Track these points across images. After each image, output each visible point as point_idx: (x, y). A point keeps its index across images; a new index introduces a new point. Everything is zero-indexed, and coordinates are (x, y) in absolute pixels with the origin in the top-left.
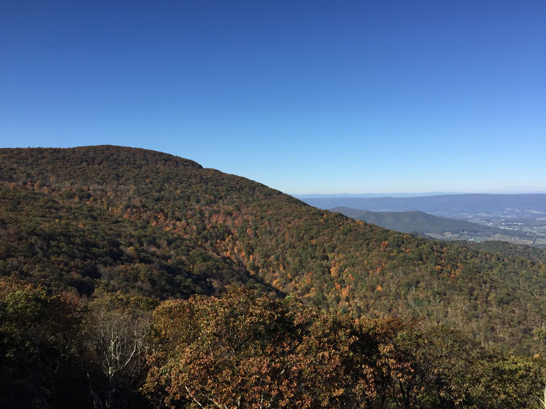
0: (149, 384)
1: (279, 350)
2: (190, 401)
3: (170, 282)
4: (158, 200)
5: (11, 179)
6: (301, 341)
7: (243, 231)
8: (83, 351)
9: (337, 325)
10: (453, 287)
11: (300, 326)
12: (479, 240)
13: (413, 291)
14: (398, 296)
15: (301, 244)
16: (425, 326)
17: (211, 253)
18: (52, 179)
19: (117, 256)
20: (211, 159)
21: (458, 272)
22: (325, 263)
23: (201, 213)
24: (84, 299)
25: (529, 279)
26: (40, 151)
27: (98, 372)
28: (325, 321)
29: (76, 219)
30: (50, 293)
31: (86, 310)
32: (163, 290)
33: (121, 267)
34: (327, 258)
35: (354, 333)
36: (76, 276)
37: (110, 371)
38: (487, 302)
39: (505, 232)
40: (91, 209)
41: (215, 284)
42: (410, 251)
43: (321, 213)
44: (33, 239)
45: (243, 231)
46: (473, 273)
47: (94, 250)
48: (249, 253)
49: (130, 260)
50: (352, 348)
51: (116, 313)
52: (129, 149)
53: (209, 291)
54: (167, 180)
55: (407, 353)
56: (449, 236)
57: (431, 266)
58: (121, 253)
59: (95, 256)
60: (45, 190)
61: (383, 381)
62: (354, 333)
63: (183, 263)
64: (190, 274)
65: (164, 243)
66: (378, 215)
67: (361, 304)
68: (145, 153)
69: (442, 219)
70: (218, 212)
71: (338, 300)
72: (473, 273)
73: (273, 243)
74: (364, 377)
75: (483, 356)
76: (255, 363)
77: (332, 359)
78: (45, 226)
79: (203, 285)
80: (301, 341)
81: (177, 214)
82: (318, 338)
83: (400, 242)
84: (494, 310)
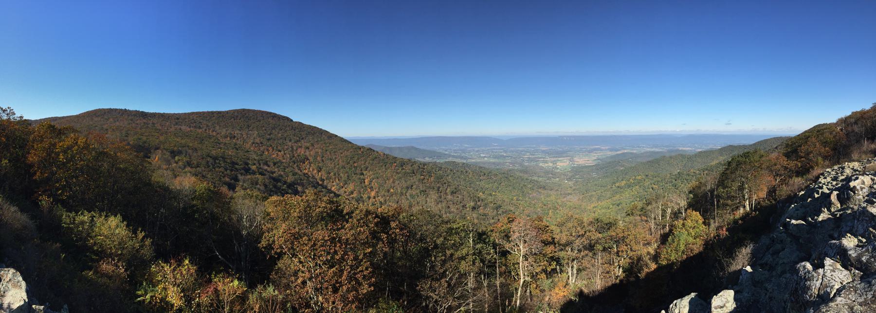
0: (264, 243)
1: (335, 227)
2: (285, 254)
3: (275, 186)
4: (269, 140)
5: (200, 128)
6: (347, 222)
7: (315, 158)
8: (230, 219)
9: (368, 213)
10: (430, 187)
11: (347, 214)
12: (442, 161)
13: (410, 191)
14: (402, 194)
15: (348, 166)
16: (415, 209)
17: (297, 171)
18: (218, 128)
19: (247, 171)
20: (297, 117)
21: (432, 179)
22: (362, 177)
23: (292, 147)
24: (231, 192)
25: (465, 180)
26: (212, 113)
27: (238, 233)
28: (361, 211)
29: (228, 149)
30: (215, 187)
31: (232, 198)
32: (271, 191)
33: (249, 177)
34: (362, 174)
35: (377, 216)
36: (227, 180)
37: (244, 232)
38: (446, 193)
39: (454, 156)
40: (236, 144)
41: (300, 189)
42: (408, 168)
43: (360, 148)
44: (209, 159)
45: (315, 158)
46: (439, 178)
47: (237, 166)
48: (319, 171)
49: (254, 173)
50: (376, 224)
51: (247, 201)
52: (254, 111)
53: (296, 193)
54: (273, 128)
55: (405, 225)
56: (427, 160)
57: (419, 176)
58: (250, 169)
59: (237, 170)
60: (214, 134)
61: (392, 242)
62: (377, 216)
63: (281, 176)
64: (285, 183)
65: (271, 164)
66: (390, 149)
67: (382, 200)
68: (262, 113)
69: (424, 150)
70: (301, 147)
71: (369, 198)
72: (439, 178)
73: (333, 165)
74: (382, 240)
75: (443, 222)
76: (321, 233)
77: (364, 233)
78: (214, 153)
79: (293, 189)
80: (347, 222)
81: (279, 148)
82: (358, 220)
83: (403, 164)
84: (449, 197)
